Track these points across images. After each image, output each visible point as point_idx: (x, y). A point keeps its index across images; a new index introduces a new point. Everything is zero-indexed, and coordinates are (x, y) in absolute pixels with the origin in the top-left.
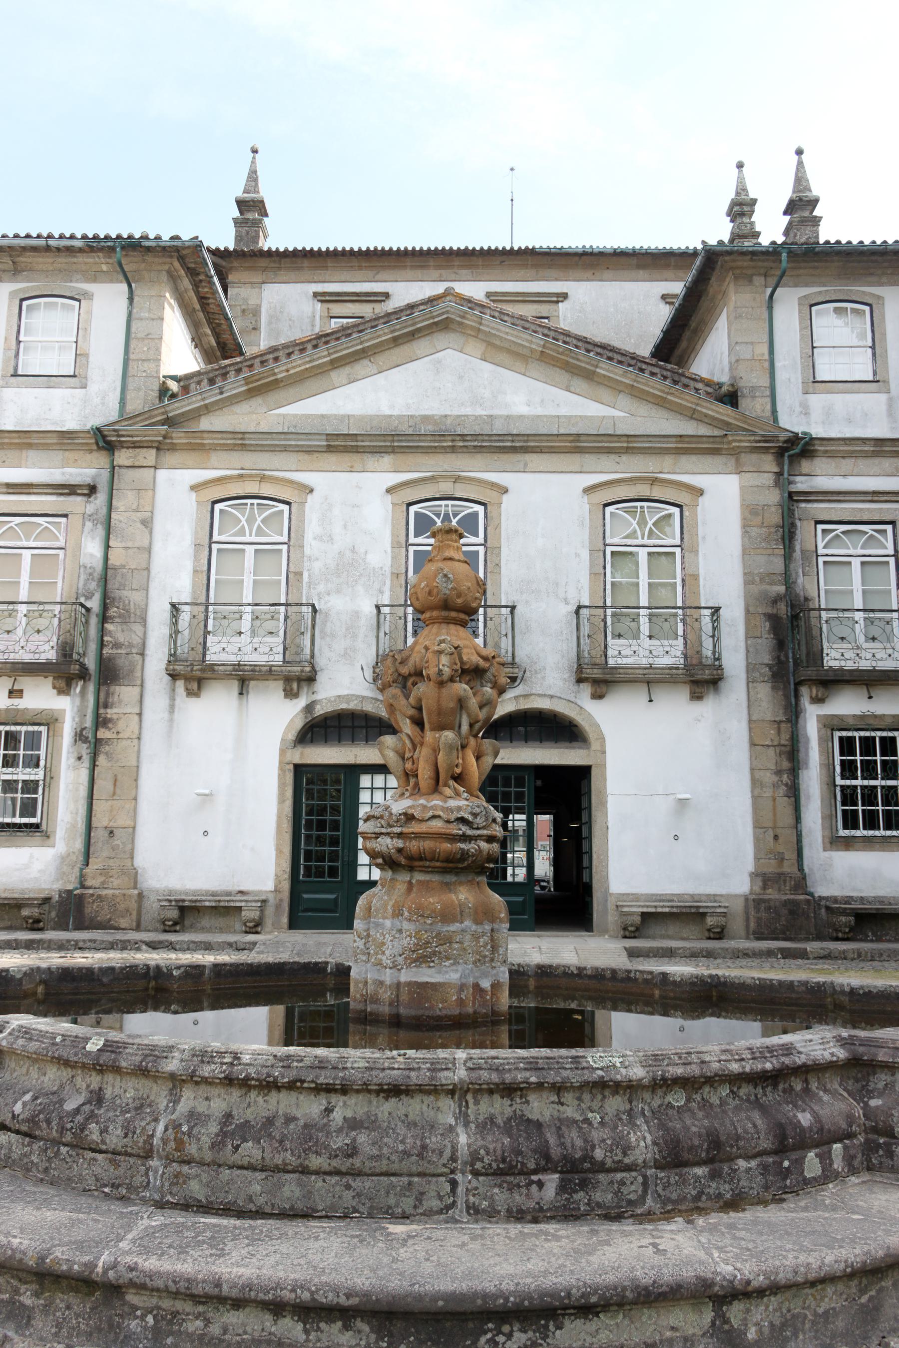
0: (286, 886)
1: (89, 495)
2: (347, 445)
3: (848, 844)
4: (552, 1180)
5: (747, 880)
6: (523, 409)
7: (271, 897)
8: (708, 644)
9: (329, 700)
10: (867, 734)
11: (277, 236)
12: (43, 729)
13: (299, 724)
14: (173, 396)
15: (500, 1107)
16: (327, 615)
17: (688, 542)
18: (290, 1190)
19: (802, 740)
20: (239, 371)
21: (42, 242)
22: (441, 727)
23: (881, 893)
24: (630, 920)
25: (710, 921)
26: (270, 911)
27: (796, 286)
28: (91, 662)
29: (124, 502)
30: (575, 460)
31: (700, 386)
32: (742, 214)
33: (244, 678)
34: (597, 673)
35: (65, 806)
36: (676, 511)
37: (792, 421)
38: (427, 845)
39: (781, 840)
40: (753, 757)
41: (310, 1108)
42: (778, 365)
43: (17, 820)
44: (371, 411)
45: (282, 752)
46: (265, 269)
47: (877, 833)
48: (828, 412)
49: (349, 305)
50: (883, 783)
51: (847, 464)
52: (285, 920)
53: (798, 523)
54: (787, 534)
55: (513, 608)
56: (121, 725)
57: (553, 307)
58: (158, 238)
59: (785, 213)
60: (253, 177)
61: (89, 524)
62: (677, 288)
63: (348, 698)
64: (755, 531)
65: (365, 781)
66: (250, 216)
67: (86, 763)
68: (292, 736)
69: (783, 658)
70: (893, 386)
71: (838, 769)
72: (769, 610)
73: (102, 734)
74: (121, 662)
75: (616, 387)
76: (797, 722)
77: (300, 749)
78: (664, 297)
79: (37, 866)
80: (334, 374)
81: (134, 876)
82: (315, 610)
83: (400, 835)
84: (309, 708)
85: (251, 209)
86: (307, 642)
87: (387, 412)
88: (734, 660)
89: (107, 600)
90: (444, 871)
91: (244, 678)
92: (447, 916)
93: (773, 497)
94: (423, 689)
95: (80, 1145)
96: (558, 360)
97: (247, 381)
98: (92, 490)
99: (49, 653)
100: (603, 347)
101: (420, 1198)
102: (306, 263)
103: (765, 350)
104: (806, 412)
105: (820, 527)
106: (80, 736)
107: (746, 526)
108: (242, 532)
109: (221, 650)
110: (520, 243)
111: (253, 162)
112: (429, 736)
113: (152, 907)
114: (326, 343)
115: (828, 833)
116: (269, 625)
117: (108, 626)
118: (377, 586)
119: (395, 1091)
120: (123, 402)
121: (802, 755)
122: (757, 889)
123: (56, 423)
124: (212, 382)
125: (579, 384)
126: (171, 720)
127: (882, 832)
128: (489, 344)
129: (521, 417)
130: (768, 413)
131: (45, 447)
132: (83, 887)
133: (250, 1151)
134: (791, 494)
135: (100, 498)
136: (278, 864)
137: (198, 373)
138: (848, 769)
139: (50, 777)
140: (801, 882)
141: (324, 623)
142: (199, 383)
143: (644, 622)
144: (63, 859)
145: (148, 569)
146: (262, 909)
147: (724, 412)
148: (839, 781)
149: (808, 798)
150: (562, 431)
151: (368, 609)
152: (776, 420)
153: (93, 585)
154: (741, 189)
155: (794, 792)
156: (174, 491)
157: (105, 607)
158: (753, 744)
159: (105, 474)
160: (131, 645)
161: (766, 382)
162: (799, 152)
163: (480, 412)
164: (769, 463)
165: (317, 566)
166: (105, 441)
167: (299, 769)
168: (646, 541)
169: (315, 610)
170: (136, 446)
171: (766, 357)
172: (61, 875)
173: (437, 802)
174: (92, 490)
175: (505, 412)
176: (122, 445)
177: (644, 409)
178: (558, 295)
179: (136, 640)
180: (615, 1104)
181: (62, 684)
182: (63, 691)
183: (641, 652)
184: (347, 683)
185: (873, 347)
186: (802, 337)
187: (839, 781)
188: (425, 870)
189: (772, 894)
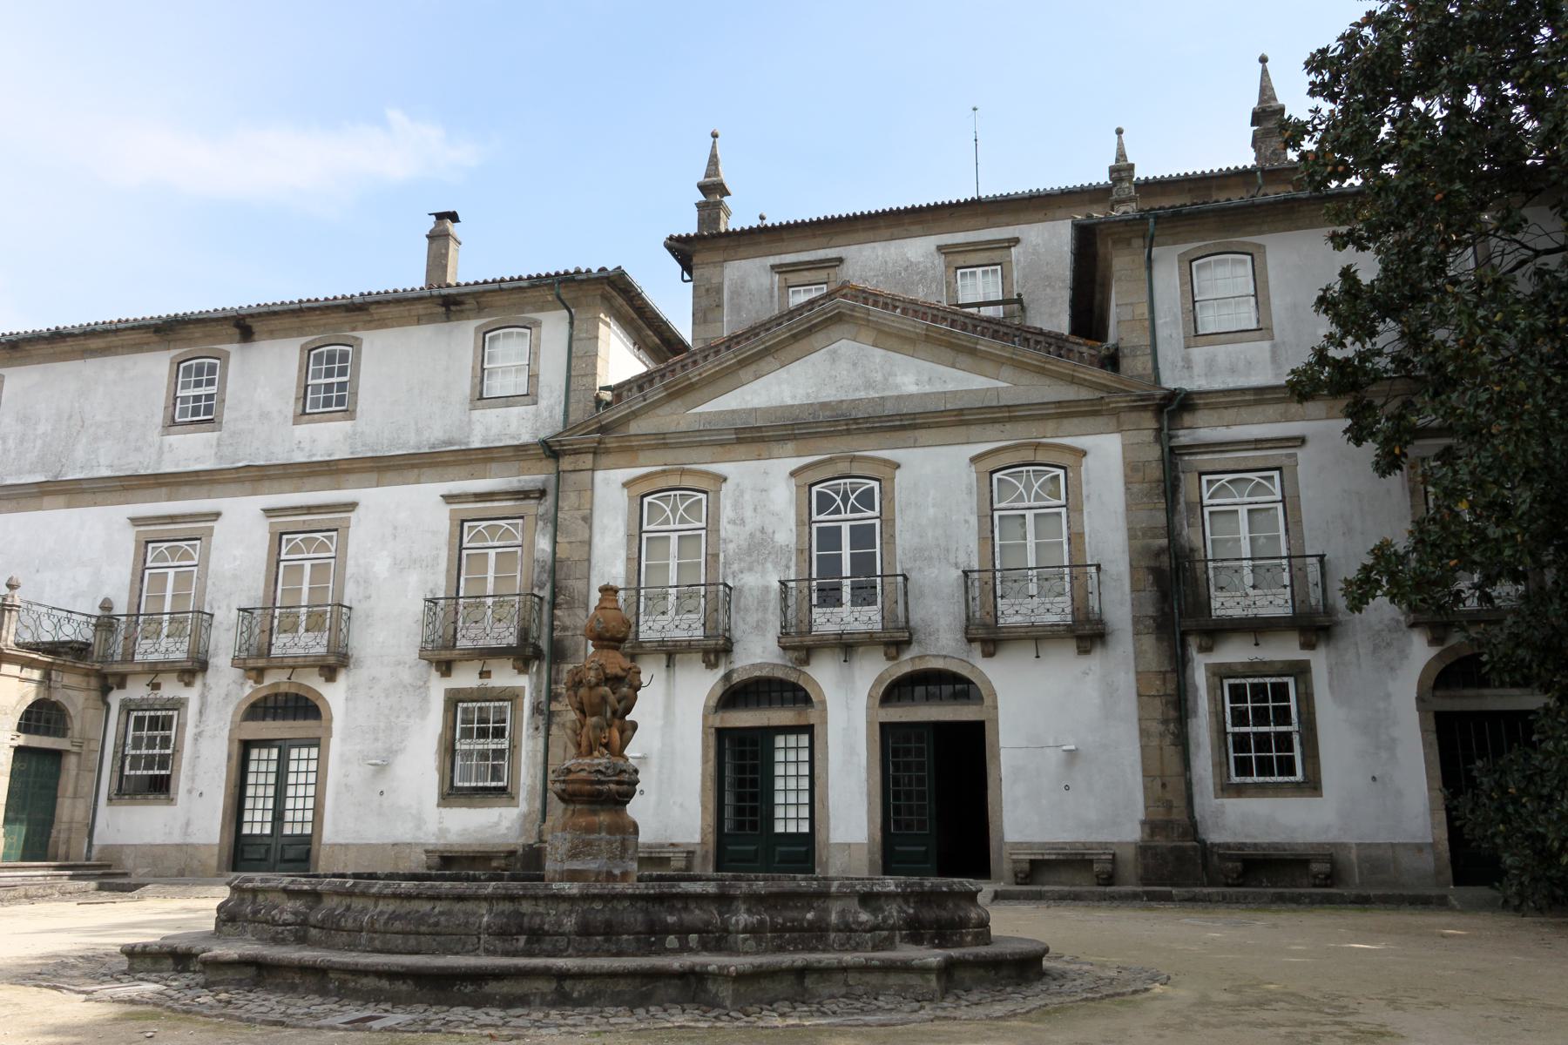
0: (711, 839)
1: (540, 498)
3: (1239, 791)
4: (523, 939)
5: (1138, 828)
6: (912, 389)
7: (698, 849)
9: (744, 669)
10: (1237, 681)
11: (739, 216)
13: (719, 692)
14: (608, 404)
15: (507, 907)
16: (741, 591)
17: (1074, 506)
18: (412, 941)
19: (1190, 689)
20: (663, 376)
21: (496, 286)
23: (1276, 839)
27: (1175, 243)
28: (544, 644)
36: (1061, 472)
37: (1172, 380)
38: (577, 786)
39: (1169, 788)
40: (1141, 707)
41: (426, 907)
42: (1159, 322)
43: (488, 784)
44: (774, 404)
45: (705, 717)
46: (725, 248)
48: (1211, 364)
50: (1255, 729)
51: (1230, 414)
53: (1182, 476)
54: (1170, 488)
57: (1005, 252)
58: (589, 271)
60: (713, 161)
61: (541, 523)
63: (761, 666)
64: (1136, 488)
65: (780, 741)
67: (542, 733)
68: (713, 703)
69: (1167, 609)
70: (1276, 331)
72: (1152, 564)
73: (555, 706)
74: (567, 643)
75: (999, 361)
76: (1184, 672)
77: (720, 714)
79: (505, 824)
84: (727, 677)
85: (713, 190)
87: (790, 402)
90: (590, 803)
92: (590, 829)
93: (1154, 452)
94: (583, 691)
95: (339, 929)
97: (666, 387)
98: (542, 493)
99: (511, 640)
101: (464, 944)
102: (763, 238)
103: (1145, 309)
104: (1188, 365)
105: (1205, 478)
106: (536, 709)
107: (1128, 483)
108: (667, 521)
111: (714, 147)
117: (557, 612)
118: (784, 562)
119: (460, 898)
121: (1190, 704)
123: (513, 438)
125: (964, 359)
127: (1255, 779)
128: (880, 331)
129: (911, 396)
130: (1149, 370)
131: (504, 459)
132: (541, 841)
133: (398, 925)
134: (1172, 449)
135: (549, 500)
139: (514, 747)
140: (1191, 828)
141: (739, 598)
144: (525, 817)
145: (589, 560)
146: (267, 851)
149: (1198, 746)
150: (949, 407)
153: (545, 577)
154: (1121, 155)
155: (1182, 742)
156: (610, 488)
157: (554, 595)
158: (1139, 695)
159: (553, 478)
160: (576, 628)
161: (1146, 341)
162: (1263, 60)
163: (873, 394)
164: (1149, 421)
165: (731, 547)
166: (551, 450)
167: (884, 727)
168: (1033, 504)
170: (576, 452)
171: (1147, 316)
172: (524, 831)
173: (587, 761)
174: (542, 493)
175: (895, 393)
176: (565, 453)
177: (1027, 379)
178: (1009, 240)
180: (564, 906)
181: (520, 664)
185: (1255, 295)
186: (1183, 293)
187: (1230, 728)
188: (582, 803)
189: (1160, 841)
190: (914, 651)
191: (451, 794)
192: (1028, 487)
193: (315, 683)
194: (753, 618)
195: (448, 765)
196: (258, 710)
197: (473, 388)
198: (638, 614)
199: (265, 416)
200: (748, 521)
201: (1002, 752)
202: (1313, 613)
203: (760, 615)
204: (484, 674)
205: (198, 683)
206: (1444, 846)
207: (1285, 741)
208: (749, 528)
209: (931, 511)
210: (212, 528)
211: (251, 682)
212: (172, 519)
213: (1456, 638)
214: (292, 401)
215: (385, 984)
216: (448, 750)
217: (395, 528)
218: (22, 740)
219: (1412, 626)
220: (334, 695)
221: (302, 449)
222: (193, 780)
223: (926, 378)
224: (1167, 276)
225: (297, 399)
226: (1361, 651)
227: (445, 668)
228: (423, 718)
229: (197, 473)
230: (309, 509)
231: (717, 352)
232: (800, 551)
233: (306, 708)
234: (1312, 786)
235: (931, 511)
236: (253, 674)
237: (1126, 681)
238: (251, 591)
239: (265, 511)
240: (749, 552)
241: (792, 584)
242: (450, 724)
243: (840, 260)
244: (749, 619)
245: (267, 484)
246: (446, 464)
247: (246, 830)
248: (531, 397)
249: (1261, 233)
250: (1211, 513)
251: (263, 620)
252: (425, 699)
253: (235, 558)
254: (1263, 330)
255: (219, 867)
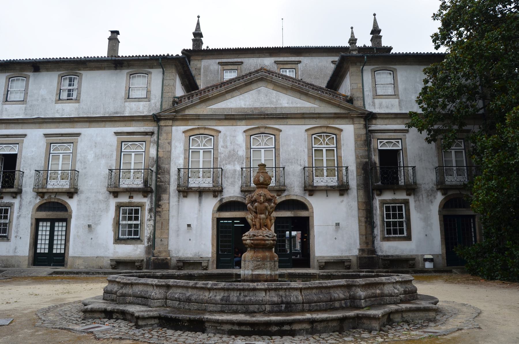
0: (215, 255)
1: (152, 135)
2: (231, 118)
6: (286, 105)
8: (345, 178)
12: (140, 208)
13: (218, 205)
20: (197, 95)
21: (137, 58)
22: (261, 214)
24: (321, 264)
25: (346, 264)
26: (210, 263)
28: (153, 187)
29: (163, 137)
30: (302, 121)
31: (341, 97)
32: (353, 43)
33: (201, 192)
34: (310, 188)
35: (147, 232)
37: (370, 108)
42: (365, 90)
45: (213, 214)
46: (202, 55)
47: (397, 236)
49: (230, 66)
51: (387, 121)
52: (215, 266)
55: (284, 168)
56: (163, 206)
57: (296, 65)
59: (371, 34)
61: (152, 144)
62: (337, 59)
63: (233, 197)
64: (359, 143)
66: (197, 38)
68: (216, 209)
70: (400, 97)
71: (385, 216)
75: (315, 98)
77: (218, 213)
78: (332, 62)
79: (139, 250)
80: (227, 95)
81: (168, 252)
82: (222, 170)
83: (252, 240)
84: (221, 200)
86: (220, 180)
87: (244, 106)
88: (353, 183)
89: (159, 167)
91: (201, 192)
93: (363, 132)
96: (296, 90)
100: (311, 85)
103: (361, 85)
104: (374, 104)
105: (379, 141)
106: (150, 210)
107: (356, 141)
109: (193, 183)
110: (285, 45)
112: (258, 216)
113: (174, 262)
114: (224, 85)
115: (382, 236)
116: (208, 175)
118: (241, 162)
120: (161, 105)
122: (360, 253)
123: (141, 113)
124: (189, 98)
126: (179, 205)
127: (398, 235)
130: (362, 105)
131: (138, 121)
135: (155, 137)
136: (213, 249)
137: (185, 96)
138: (388, 216)
139: (142, 223)
142: (185, 99)
143: (325, 171)
146: (208, 263)
147: (348, 105)
148: (385, 220)
150: (298, 112)
151: (238, 168)
152: (365, 107)
156: (178, 132)
160: (165, 182)
163: (272, 106)
164: (362, 122)
165: (222, 155)
166: (156, 119)
167: (218, 219)
169: (222, 170)
174: (152, 133)
179: (167, 180)
182: (145, 196)
183: (324, 181)
184: (232, 191)
186: (372, 81)
187: (385, 220)
190: (286, 193)
191: (118, 240)
192: (324, 140)
193: (65, 199)
194: (230, 180)
195: (117, 229)
196: (41, 208)
197: (125, 94)
198: (120, 178)
199: (44, 100)
200: (228, 147)
201: (315, 227)
202: (411, 185)
203: (233, 179)
204: (131, 197)
205: (18, 197)
206: (445, 255)
207: (401, 224)
208: (229, 149)
209: (292, 147)
210: (23, 140)
211: (39, 197)
212: (7, 136)
213: (450, 193)
214: (55, 95)
215: (236, 328)
216: (117, 224)
217: (96, 143)
218: (218, 215)
219: (438, 189)
220: (73, 204)
221: (59, 113)
222: (17, 232)
223: (290, 102)
224: (367, 77)
225: (57, 94)
226: (424, 196)
227: (115, 194)
228: (107, 212)
229: (17, 119)
230: (62, 135)
231: (217, 88)
232: (247, 158)
233: (64, 208)
234: (409, 238)
235: (292, 147)
236: (41, 195)
237: (355, 204)
238: (40, 164)
239: (44, 135)
240: (229, 158)
241: (245, 169)
242: (118, 215)
243: (242, 63)
244: (229, 181)
245: (45, 125)
246: (116, 121)
247: (38, 251)
248: (148, 98)
249: (395, 65)
250: (315, 150)
251: (43, 174)
252: (108, 206)
253: (32, 152)
254: (396, 95)
255: (28, 265)
